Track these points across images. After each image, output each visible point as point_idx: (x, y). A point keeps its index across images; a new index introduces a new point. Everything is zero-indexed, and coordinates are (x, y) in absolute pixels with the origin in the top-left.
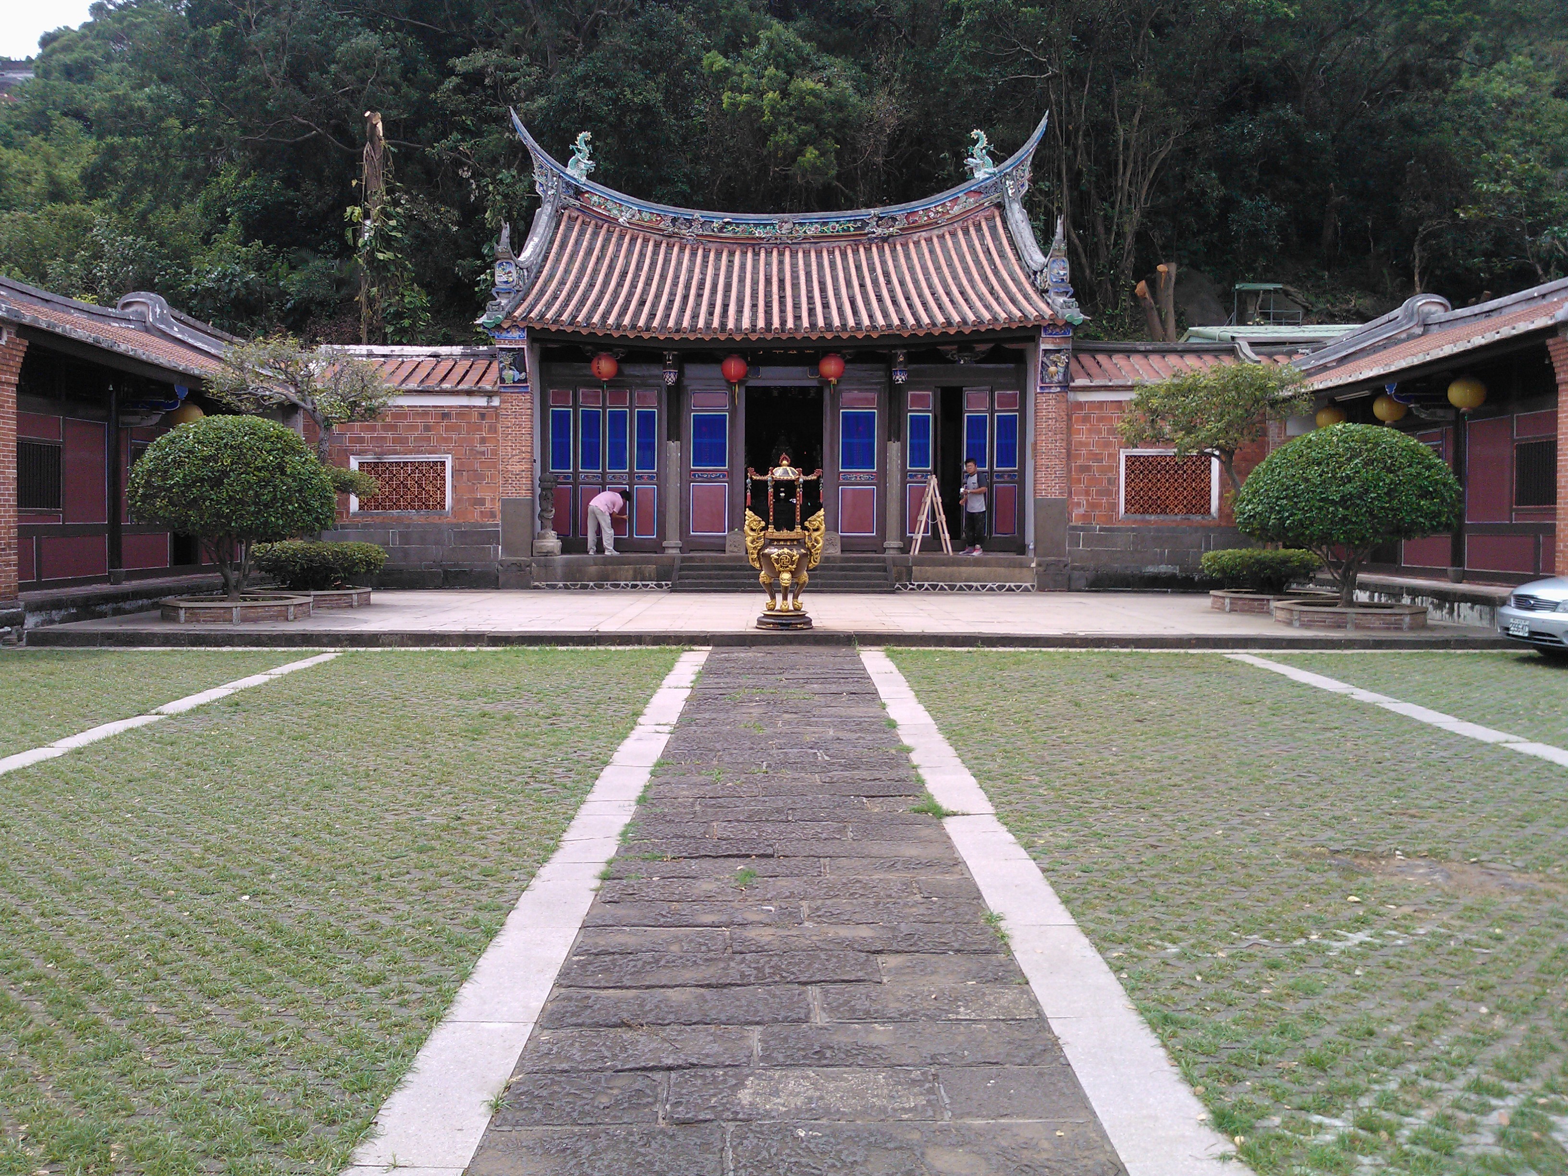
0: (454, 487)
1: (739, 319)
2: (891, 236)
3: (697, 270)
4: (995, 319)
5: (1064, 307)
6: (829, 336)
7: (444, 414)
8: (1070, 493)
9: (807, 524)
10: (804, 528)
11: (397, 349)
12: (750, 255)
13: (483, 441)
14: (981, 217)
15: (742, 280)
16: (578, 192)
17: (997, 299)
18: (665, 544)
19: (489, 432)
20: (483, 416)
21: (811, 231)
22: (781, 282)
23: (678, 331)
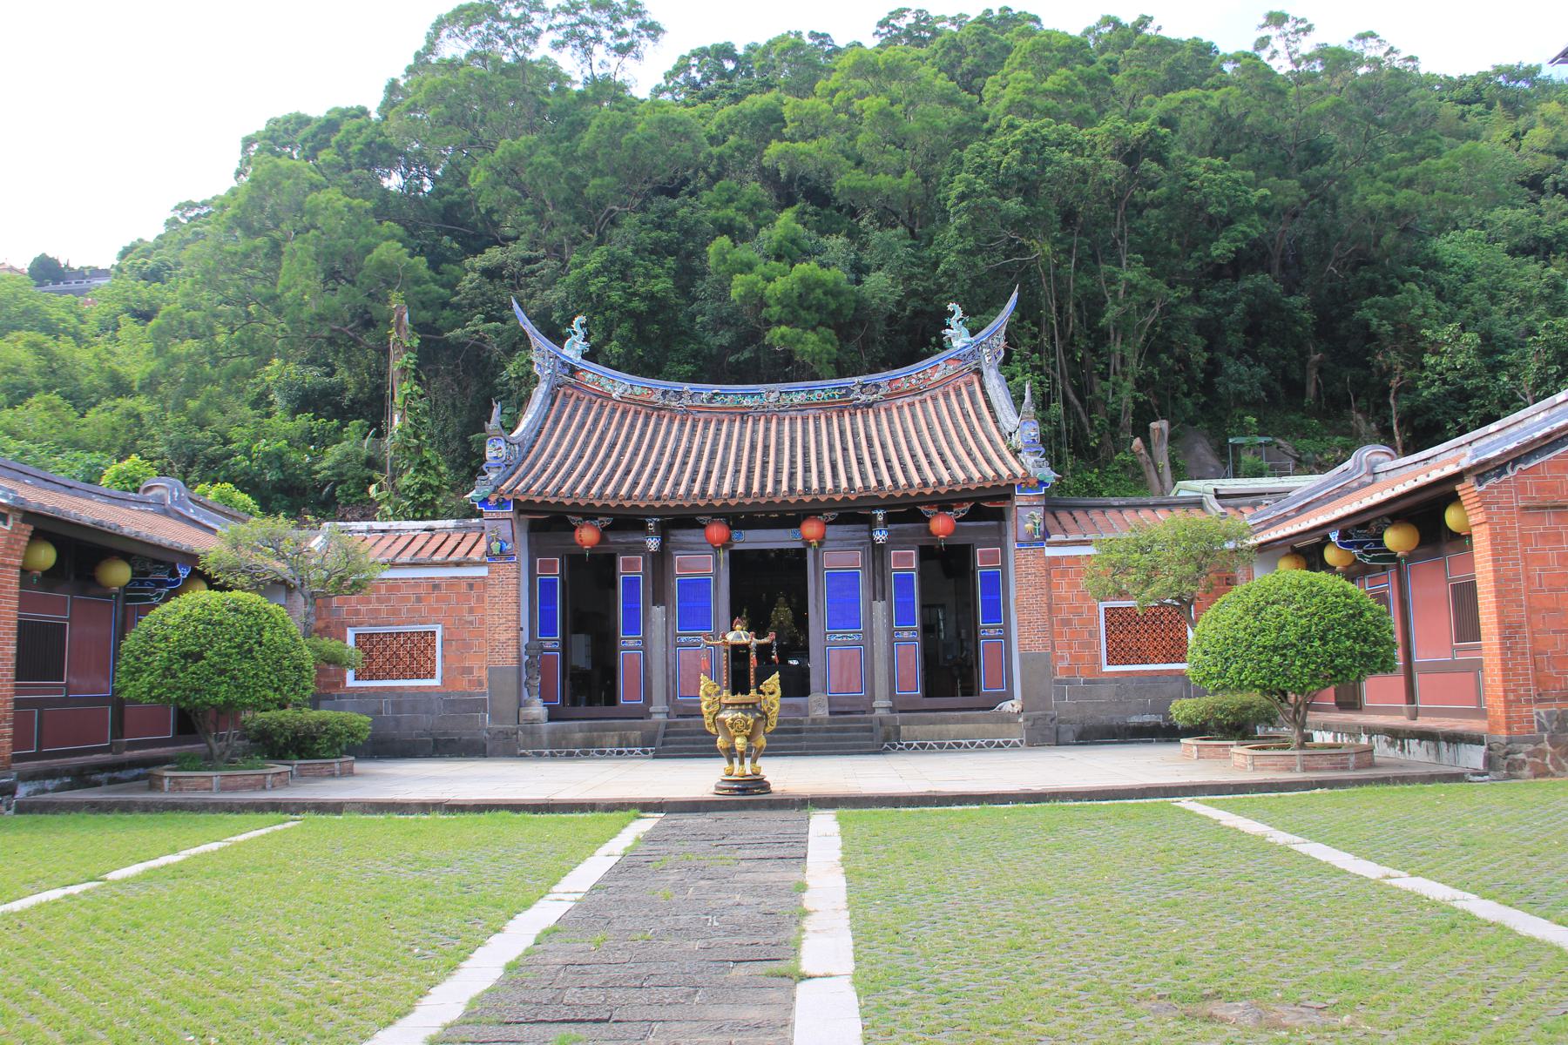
0: (443, 656)
1: (719, 486)
3: (685, 439)
4: (970, 479)
5: (1032, 464)
6: (807, 499)
7: (435, 586)
8: (1053, 648)
11: (395, 524)
12: (737, 424)
13: (471, 610)
14: (961, 382)
15: (727, 447)
16: (573, 371)
17: (974, 460)
20: (471, 586)
21: (798, 399)
22: (766, 447)
23: (658, 498)
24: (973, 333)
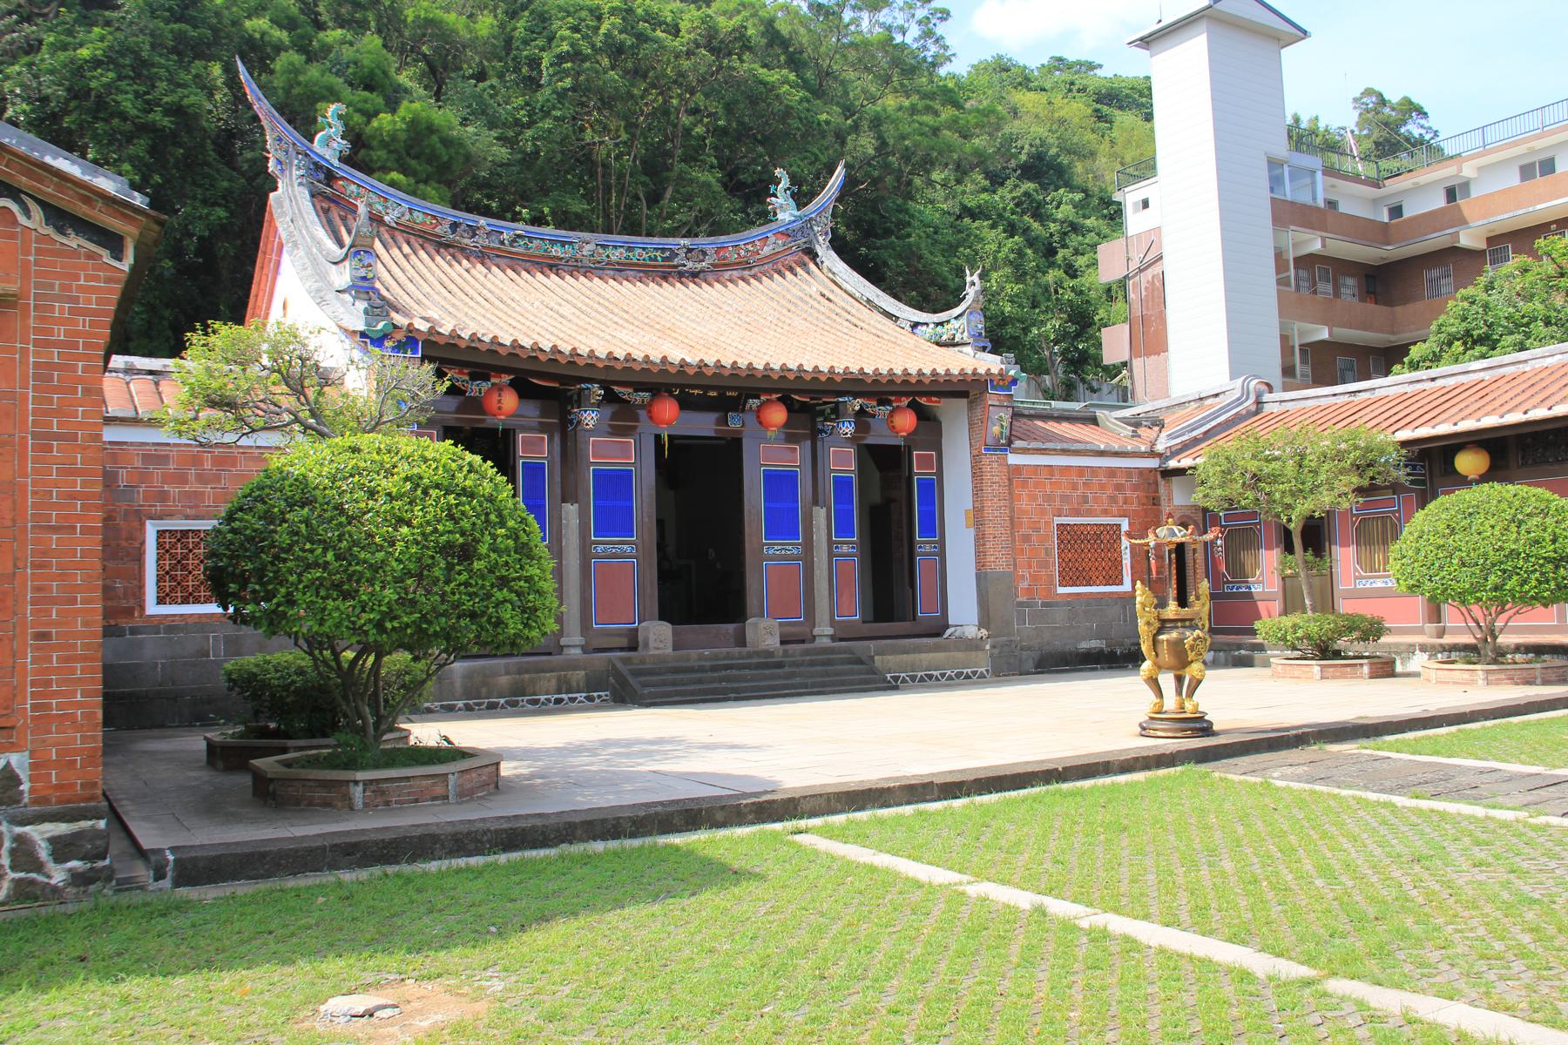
2: (702, 271)
21: (616, 255)
24: (800, 206)
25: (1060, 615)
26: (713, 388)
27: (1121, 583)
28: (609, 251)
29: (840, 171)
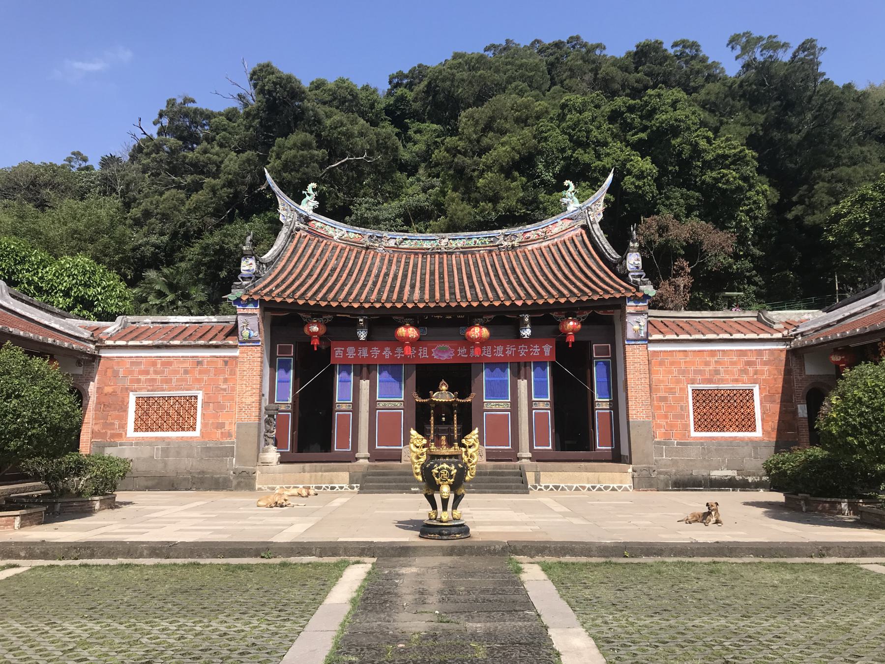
0: (203, 415)
8: (654, 417)
9: (464, 441)
10: (462, 445)
16: (307, 220)
18: (357, 455)
19: (230, 375)
20: (226, 363)
25: (694, 453)
26: (449, 314)
27: (754, 430)
28: (457, 242)
29: (611, 176)
